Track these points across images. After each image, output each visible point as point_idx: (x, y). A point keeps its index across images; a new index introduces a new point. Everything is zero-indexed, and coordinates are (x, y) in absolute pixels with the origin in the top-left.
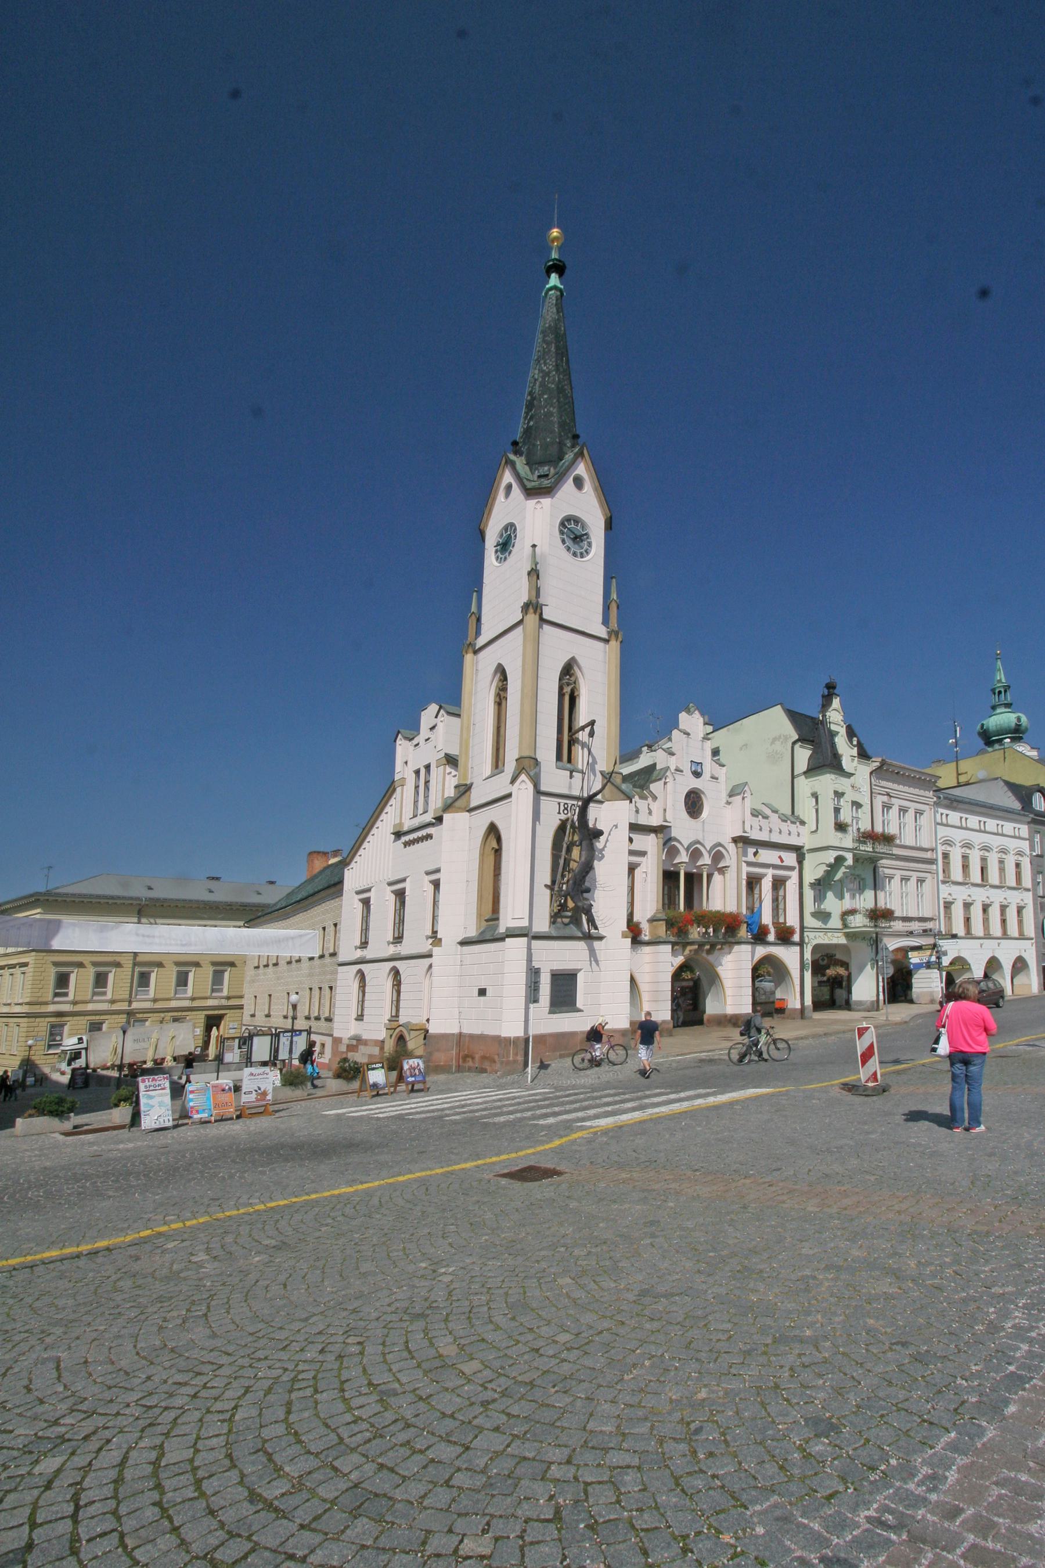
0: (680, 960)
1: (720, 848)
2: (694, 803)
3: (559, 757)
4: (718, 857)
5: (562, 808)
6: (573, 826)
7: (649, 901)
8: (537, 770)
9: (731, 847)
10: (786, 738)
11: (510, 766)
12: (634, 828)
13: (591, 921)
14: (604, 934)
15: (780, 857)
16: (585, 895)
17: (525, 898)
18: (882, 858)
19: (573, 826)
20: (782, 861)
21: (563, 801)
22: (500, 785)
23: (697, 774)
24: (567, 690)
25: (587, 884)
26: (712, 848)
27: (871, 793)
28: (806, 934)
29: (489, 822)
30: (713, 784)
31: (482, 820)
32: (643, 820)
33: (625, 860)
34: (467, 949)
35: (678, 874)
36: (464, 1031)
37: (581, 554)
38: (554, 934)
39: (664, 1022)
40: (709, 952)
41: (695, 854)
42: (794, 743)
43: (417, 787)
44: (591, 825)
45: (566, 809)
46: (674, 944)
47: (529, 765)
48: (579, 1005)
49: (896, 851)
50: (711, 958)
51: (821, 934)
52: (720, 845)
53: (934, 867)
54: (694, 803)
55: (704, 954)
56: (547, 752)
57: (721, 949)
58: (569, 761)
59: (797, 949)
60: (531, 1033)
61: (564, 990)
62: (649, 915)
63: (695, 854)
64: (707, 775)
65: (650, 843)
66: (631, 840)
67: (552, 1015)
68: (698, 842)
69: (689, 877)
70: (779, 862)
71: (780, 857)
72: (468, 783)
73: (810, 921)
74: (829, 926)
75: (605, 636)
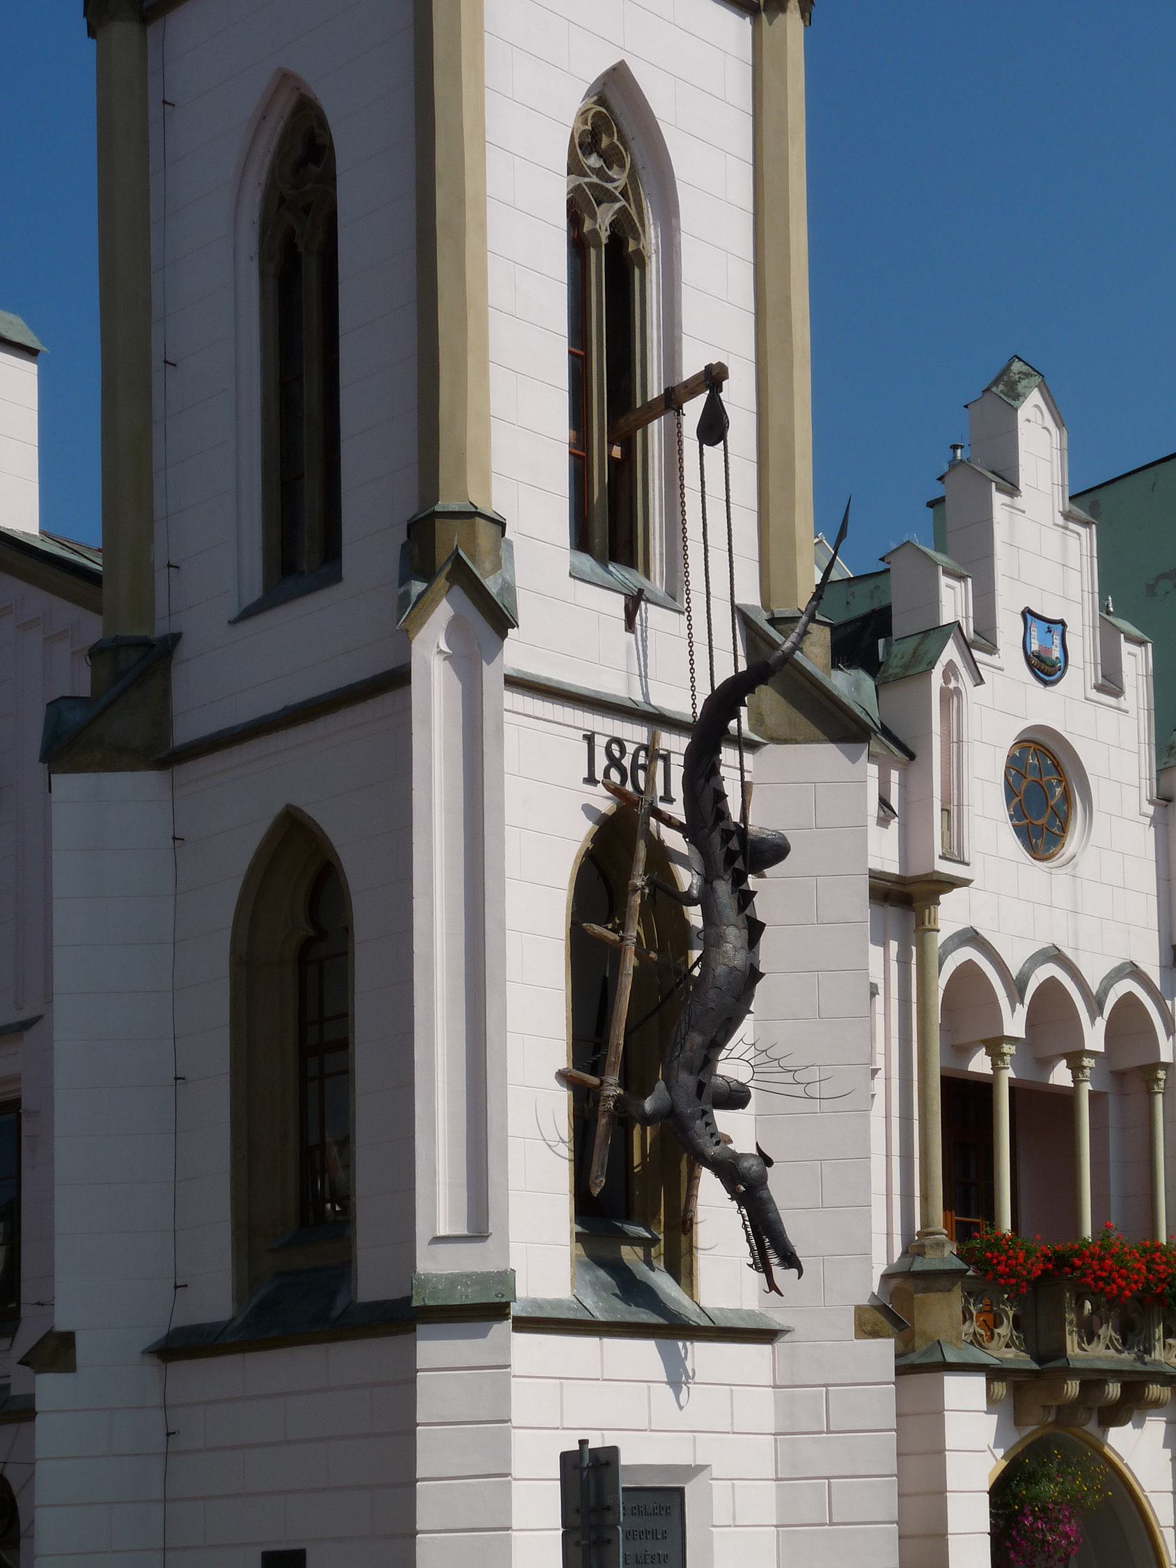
5: (601, 761)
23: (1045, 669)
24: (604, 217)
29: (277, 808)
31: (235, 807)
45: (614, 762)
72: (161, 629)
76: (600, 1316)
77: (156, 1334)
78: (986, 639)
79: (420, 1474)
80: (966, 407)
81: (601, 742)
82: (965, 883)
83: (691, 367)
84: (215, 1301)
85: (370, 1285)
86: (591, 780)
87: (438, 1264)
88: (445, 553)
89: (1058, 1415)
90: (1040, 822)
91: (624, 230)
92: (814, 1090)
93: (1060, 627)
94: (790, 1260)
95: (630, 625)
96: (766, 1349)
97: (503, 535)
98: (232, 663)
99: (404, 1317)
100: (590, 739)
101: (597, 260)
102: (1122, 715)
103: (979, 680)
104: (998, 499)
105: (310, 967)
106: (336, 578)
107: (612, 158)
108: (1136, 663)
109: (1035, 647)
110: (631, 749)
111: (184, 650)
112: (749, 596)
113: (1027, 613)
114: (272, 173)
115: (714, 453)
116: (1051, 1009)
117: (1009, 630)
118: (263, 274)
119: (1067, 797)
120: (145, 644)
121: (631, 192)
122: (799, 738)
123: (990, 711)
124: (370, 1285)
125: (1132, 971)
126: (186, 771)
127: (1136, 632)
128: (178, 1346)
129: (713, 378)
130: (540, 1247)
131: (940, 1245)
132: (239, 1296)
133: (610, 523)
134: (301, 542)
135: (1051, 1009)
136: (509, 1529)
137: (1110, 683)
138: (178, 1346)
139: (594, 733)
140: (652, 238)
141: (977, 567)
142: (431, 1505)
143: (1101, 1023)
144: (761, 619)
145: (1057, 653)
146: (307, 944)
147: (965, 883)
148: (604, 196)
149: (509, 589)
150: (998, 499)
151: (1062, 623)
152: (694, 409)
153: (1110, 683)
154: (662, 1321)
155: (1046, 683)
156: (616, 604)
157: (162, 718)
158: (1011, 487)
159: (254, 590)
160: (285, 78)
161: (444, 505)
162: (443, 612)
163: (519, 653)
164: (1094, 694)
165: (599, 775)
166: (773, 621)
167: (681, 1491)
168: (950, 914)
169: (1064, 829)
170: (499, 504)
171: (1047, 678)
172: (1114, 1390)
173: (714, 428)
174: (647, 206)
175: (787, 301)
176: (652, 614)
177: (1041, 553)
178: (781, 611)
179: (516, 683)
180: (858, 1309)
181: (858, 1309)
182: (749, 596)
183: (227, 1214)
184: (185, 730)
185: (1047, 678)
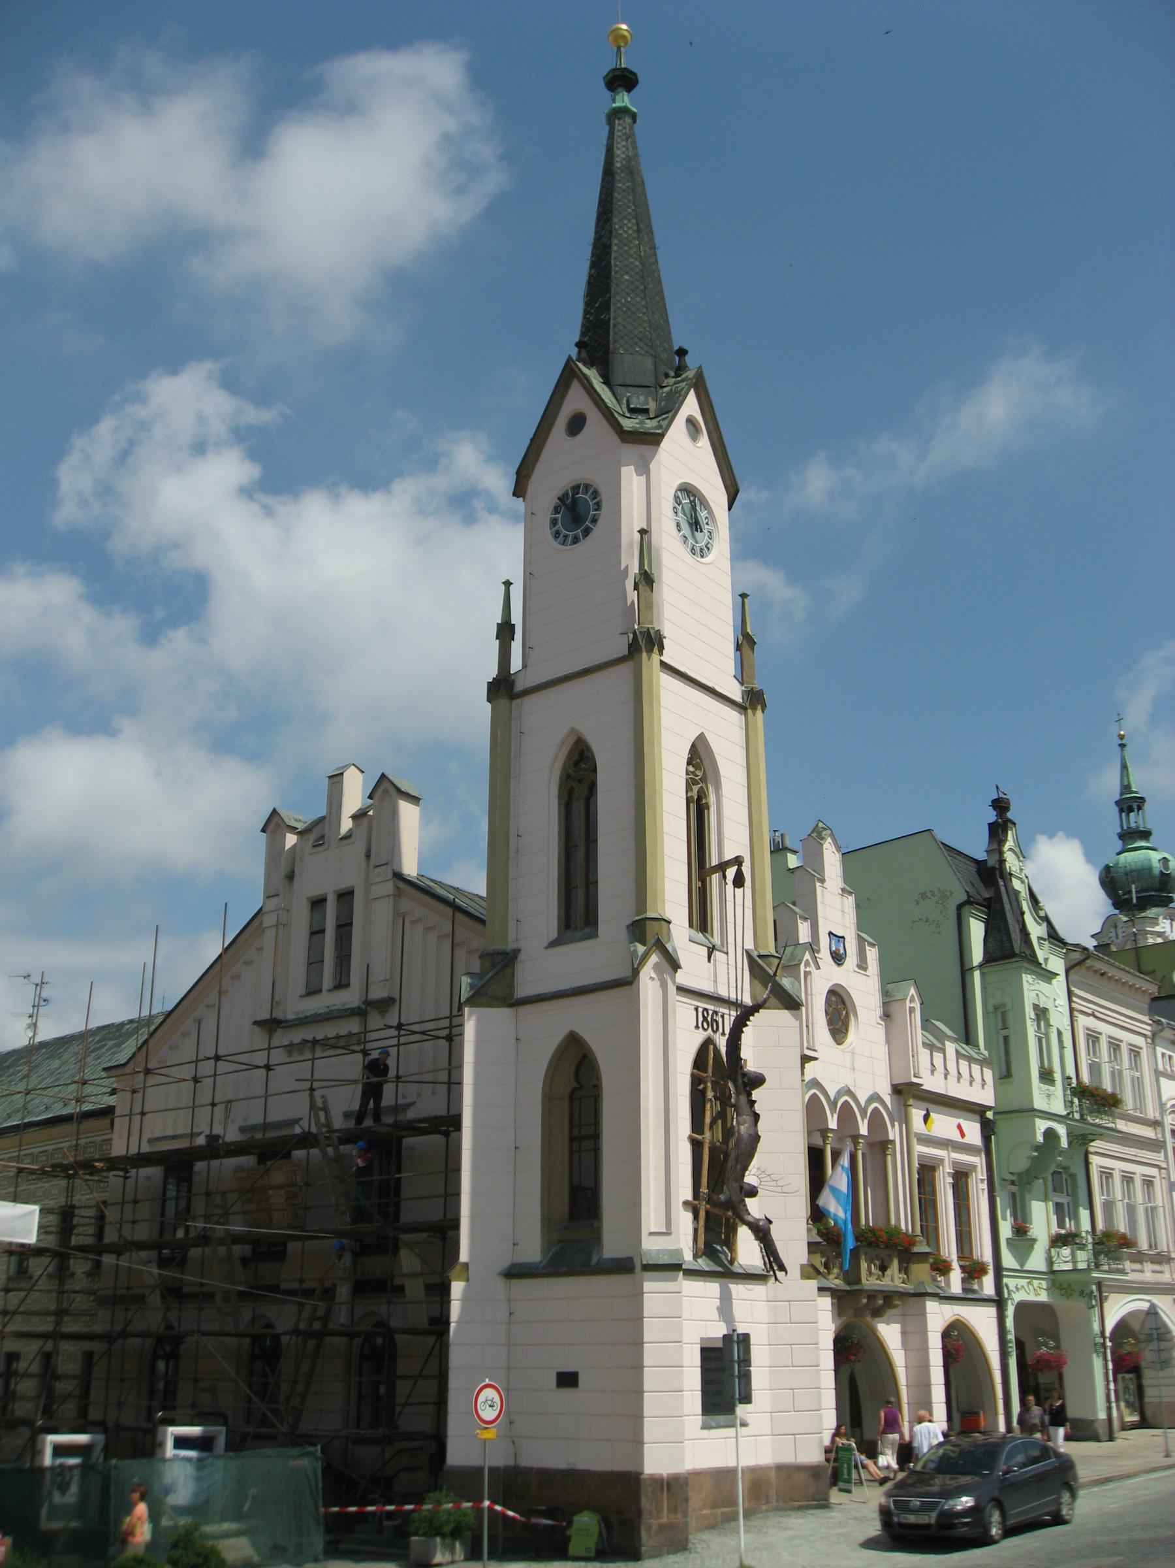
5: (701, 1019)
10: (945, 896)
15: (959, 1127)
18: (1101, 1136)
20: (963, 1135)
24: (696, 788)
26: (839, 1094)
27: (1071, 1010)
28: (1005, 1280)
29: (566, 1031)
31: (548, 1029)
34: (520, 1285)
36: (526, 1461)
37: (701, 550)
42: (960, 907)
43: (317, 932)
45: (705, 1019)
49: (1121, 1125)
51: (1024, 1282)
53: (1162, 1156)
59: (992, 1311)
70: (955, 1136)
71: (959, 1127)
72: (511, 946)
73: (1008, 1260)
74: (1026, 1268)
75: (738, 698)
77: (505, 1265)
78: (813, 947)
79: (645, 1340)
81: (700, 1010)
82: (816, 1059)
83: (729, 855)
84: (532, 1252)
85: (611, 1248)
86: (697, 1027)
87: (652, 1246)
88: (645, 930)
91: (702, 795)
95: (709, 961)
98: (544, 965)
99: (624, 1266)
100: (696, 1009)
101: (693, 806)
103: (818, 968)
104: (818, 884)
105: (580, 1104)
106: (594, 935)
107: (697, 767)
108: (872, 954)
111: (522, 956)
112: (749, 945)
113: (830, 933)
114: (565, 763)
115: (739, 891)
116: (846, 1115)
117: (824, 940)
118: (560, 804)
119: (847, 1016)
120: (505, 953)
121: (704, 779)
123: (820, 979)
124: (611, 1248)
125: (875, 1097)
126: (524, 1010)
127: (871, 940)
128: (514, 1273)
129: (738, 861)
130: (683, 1237)
132: (545, 1250)
133: (701, 920)
134: (578, 914)
135: (846, 1115)
137: (862, 965)
138: (514, 1273)
140: (712, 798)
141: (812, 917)
142: (650, 1355)
143: (866, 1121)
144: (755, 954)
145: (842, 951)
146: (574, 1091)
147: (816, 1059)
148: (695, 783)
149: (675, 951)
150: (818, 884)
152: (731, 872)
153: (862, 965)
154: (720, 1269)
156: (704, 951)
157: (511, 986)
158: (823, 881)
159: (554, 935)
160: (573, 730)
161: (650, 914)
162: (654, 958)
163: (682, 978)
166: (760, 956)
169: (847, 1030)
170: (668, 915)
173: (739, 881)
174: (710, 789)
175: (761, 823)
176: (717, 954)
177: (836, 910)
178: (763, 952)
179: (681, 990)
180: (802, 1266)
181: (802, 1266)
182: (749, 945)
183: (539, 1213)
184: (522, 991)
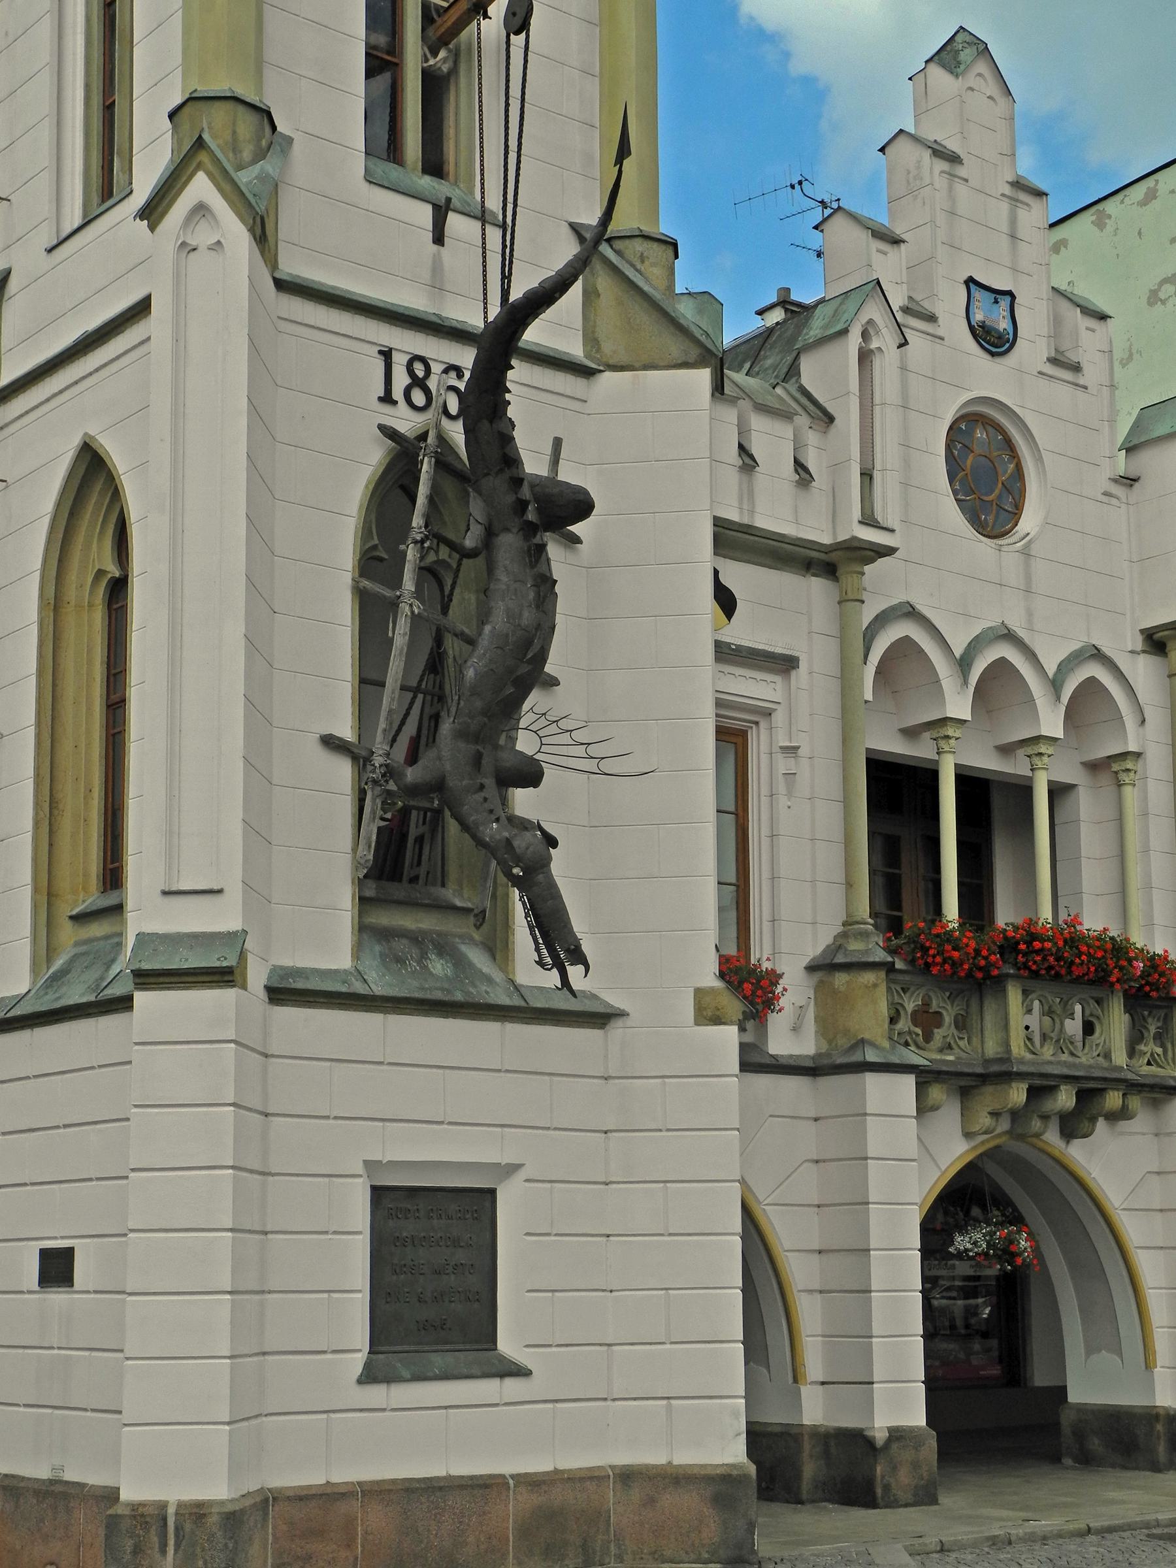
0: (951, 1150)
1: (1094, 670)
2: (987, 471)
3: (386, 145)
4: (1087, 705)
5: (401, 380)
6: (445, 463)
7: (815, 884)
8: (268, 166)
9: (1144, 672)
11: (151, 155)
12: (732, 539)
13: (558, 943)
14: (614, 999)
16: (523, 801)
17: (242, 799)
19: (445, 463)
21: (406, 342)
22: (125, 253)
23: (994, 342)
25: (525, 744)
30: (1060, 393)
32: (777, 513)
33: (704, 686)
35: (928, 777)
38: (379, 983)
39: (897, 1435)
40: (1073, 1126)
41: (996, 688)
44: (534, 465)
45: (418, 383)
46: (926, 1077)
47: (232, 133)
48: (507, 1344)
50: (1077, 1153)
52: (1098, 655)
54: (987, 471)
55: (1052, 1137)
56: (325, 102)
57: (1123, 1114)
58: (434, 166)
60: (874, 1340)
61: (433, 1275)
62: (815, 946)
63: (996, 688)
64: (1032, 349)
65: (781, 609)
66: (726, 601)
67: (377, 1394)
68: (1009, 636)
69: (973, 787)
76: (378, 990)
80: (910, 79)
81: (399, 362)
86: (387, 399)
89: (1013, 1121)
90: (990, 498)
92: (606, 766)
93: (1008, 299)
94: (578, 957)
96: (597, 1033)
97: (274, 128)
100: (387, 355)
102: (1079, 393)
109: (978, 316)
110: (436, 368)
115: (518, 40)
122: (637, 365)
131: (864, 935)
136: (871, 1337)
139: (391, 349)
147: (889, 551)
151: (1010, 293)
155: (993, 354)
156: (424, 214)
164: (1049, 369)
165: (398, 393)
167: (492, 1192)
168: (881, 585)
171: (994, 350)
172: (1066, 1099)
185: (994, 350)
